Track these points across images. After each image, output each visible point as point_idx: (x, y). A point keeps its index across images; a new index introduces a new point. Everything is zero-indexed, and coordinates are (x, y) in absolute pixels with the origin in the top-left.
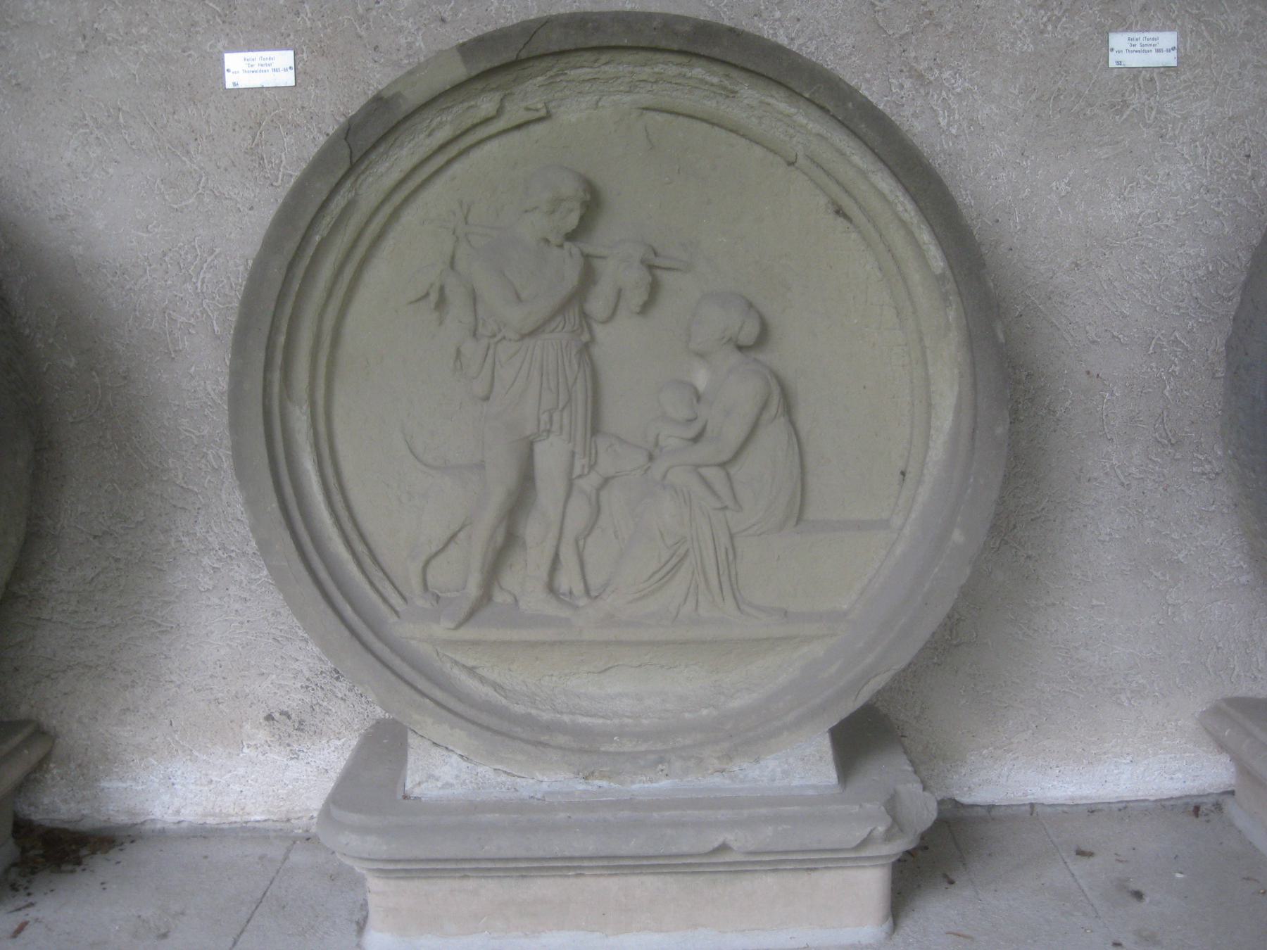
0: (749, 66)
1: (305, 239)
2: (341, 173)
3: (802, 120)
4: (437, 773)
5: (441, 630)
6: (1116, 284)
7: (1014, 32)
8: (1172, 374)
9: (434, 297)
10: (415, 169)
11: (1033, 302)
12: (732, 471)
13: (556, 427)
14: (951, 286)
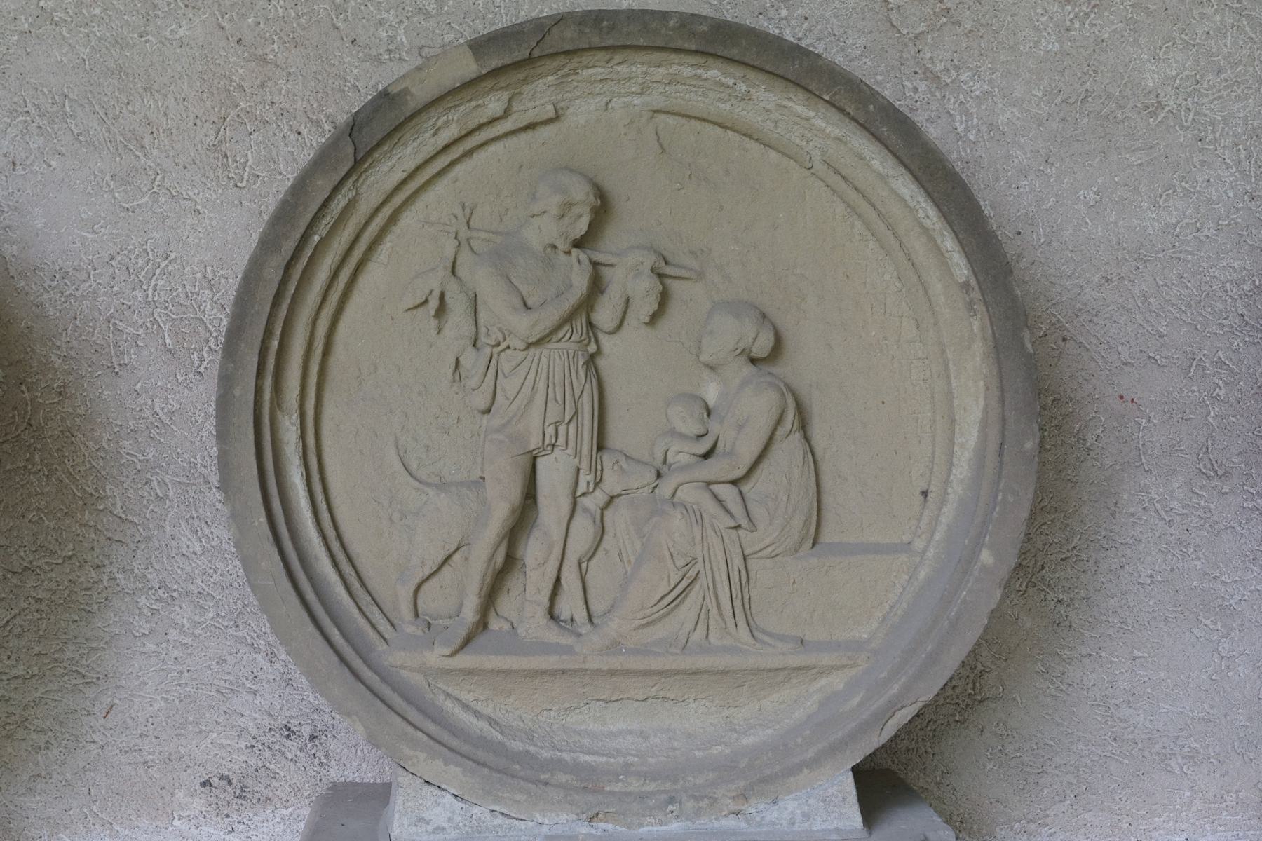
0: (767, 67)
1: (305, 238)
2: (344, 171)
3: (820, 123)
4: (427, 815)
5: (436, 657)
6: (1151, 300)
7: (1037, 29)
8: (1217, 397)
9: (434, 304)
10: (419, 168)
11: (1059, 320)
12: (746, 488)
13: (561, 440)
14: (976, 295)
